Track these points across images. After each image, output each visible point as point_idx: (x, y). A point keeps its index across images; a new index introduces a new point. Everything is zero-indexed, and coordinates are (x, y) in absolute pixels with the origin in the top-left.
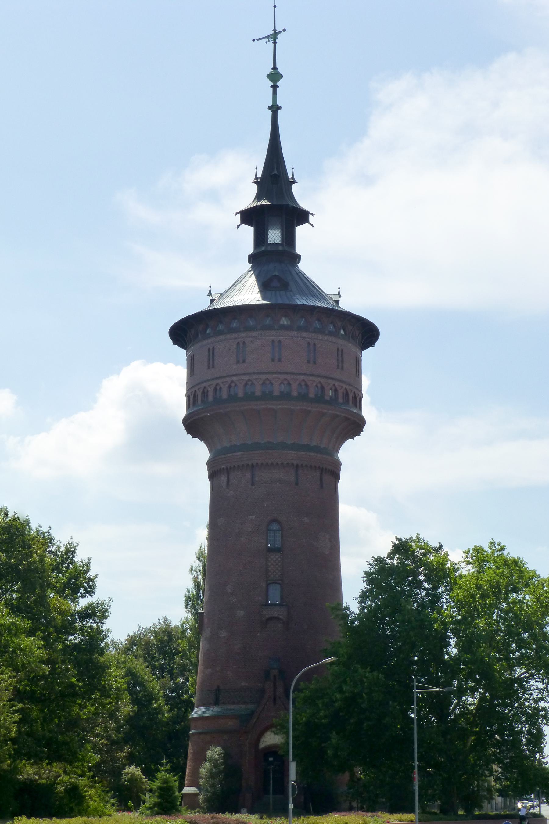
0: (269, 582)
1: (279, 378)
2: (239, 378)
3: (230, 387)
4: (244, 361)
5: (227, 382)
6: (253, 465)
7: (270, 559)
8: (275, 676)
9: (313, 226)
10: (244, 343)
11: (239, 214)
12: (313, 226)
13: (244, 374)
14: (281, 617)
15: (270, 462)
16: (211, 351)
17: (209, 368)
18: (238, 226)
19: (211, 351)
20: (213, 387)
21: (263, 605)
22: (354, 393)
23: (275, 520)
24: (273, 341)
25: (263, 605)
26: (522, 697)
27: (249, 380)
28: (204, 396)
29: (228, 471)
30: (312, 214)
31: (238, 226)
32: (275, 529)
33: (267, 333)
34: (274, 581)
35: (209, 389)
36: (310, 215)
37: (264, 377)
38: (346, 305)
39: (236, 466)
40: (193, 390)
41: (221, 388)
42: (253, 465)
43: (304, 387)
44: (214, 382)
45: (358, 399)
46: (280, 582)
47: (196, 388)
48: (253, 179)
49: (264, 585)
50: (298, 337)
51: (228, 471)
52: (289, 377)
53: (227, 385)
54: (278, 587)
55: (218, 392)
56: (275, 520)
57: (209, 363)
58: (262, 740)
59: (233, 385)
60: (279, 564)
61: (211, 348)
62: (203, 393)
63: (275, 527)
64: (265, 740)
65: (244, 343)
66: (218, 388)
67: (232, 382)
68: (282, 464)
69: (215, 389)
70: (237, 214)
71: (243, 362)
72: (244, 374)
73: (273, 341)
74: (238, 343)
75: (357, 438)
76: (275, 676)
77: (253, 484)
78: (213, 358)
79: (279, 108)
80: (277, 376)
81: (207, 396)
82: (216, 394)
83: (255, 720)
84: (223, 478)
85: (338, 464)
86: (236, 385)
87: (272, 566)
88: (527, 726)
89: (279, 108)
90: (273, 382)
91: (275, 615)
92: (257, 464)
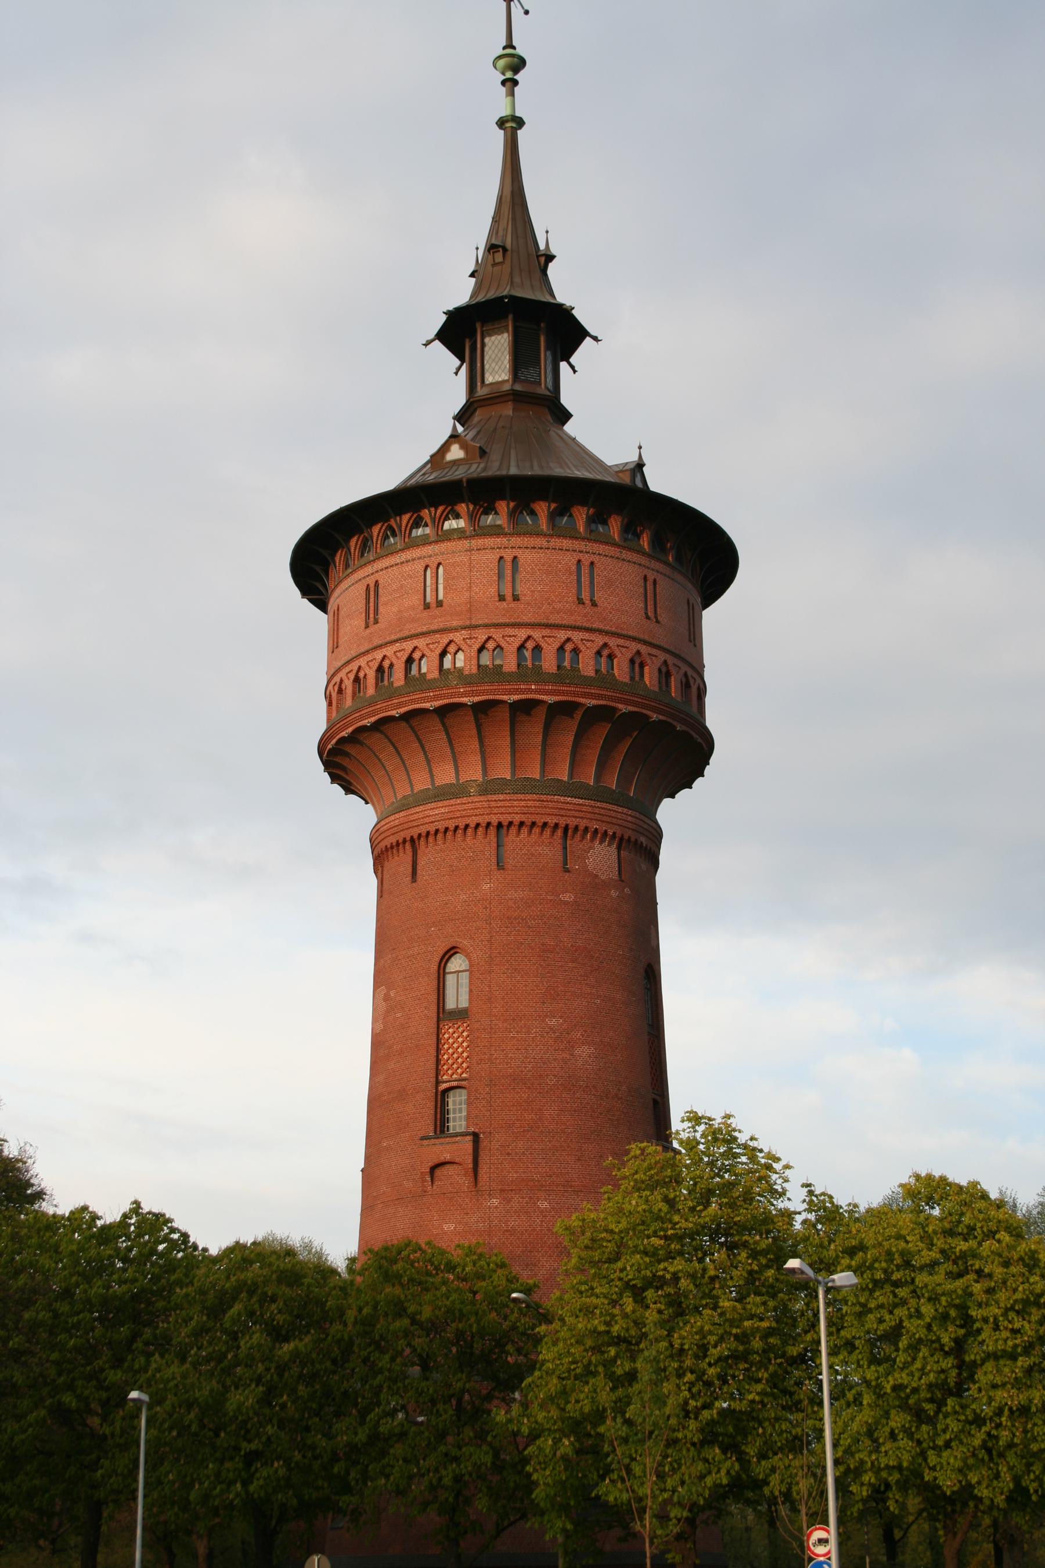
6: (500, 825)
17: (367, 627)
20: (375, 665)
22: (686, 675)
33: (489, 541)
38: (658, 482)
40: (337, 679)
41: (391, 665)
44: (409, 646)
45: (694, 689)
47: (362, 662)
53: (477, 646)
62: (357, 680)
75: (699, 782)
79: (520, 123)
84: (401, 862)
85: (657, 835)
89: (520, 123)
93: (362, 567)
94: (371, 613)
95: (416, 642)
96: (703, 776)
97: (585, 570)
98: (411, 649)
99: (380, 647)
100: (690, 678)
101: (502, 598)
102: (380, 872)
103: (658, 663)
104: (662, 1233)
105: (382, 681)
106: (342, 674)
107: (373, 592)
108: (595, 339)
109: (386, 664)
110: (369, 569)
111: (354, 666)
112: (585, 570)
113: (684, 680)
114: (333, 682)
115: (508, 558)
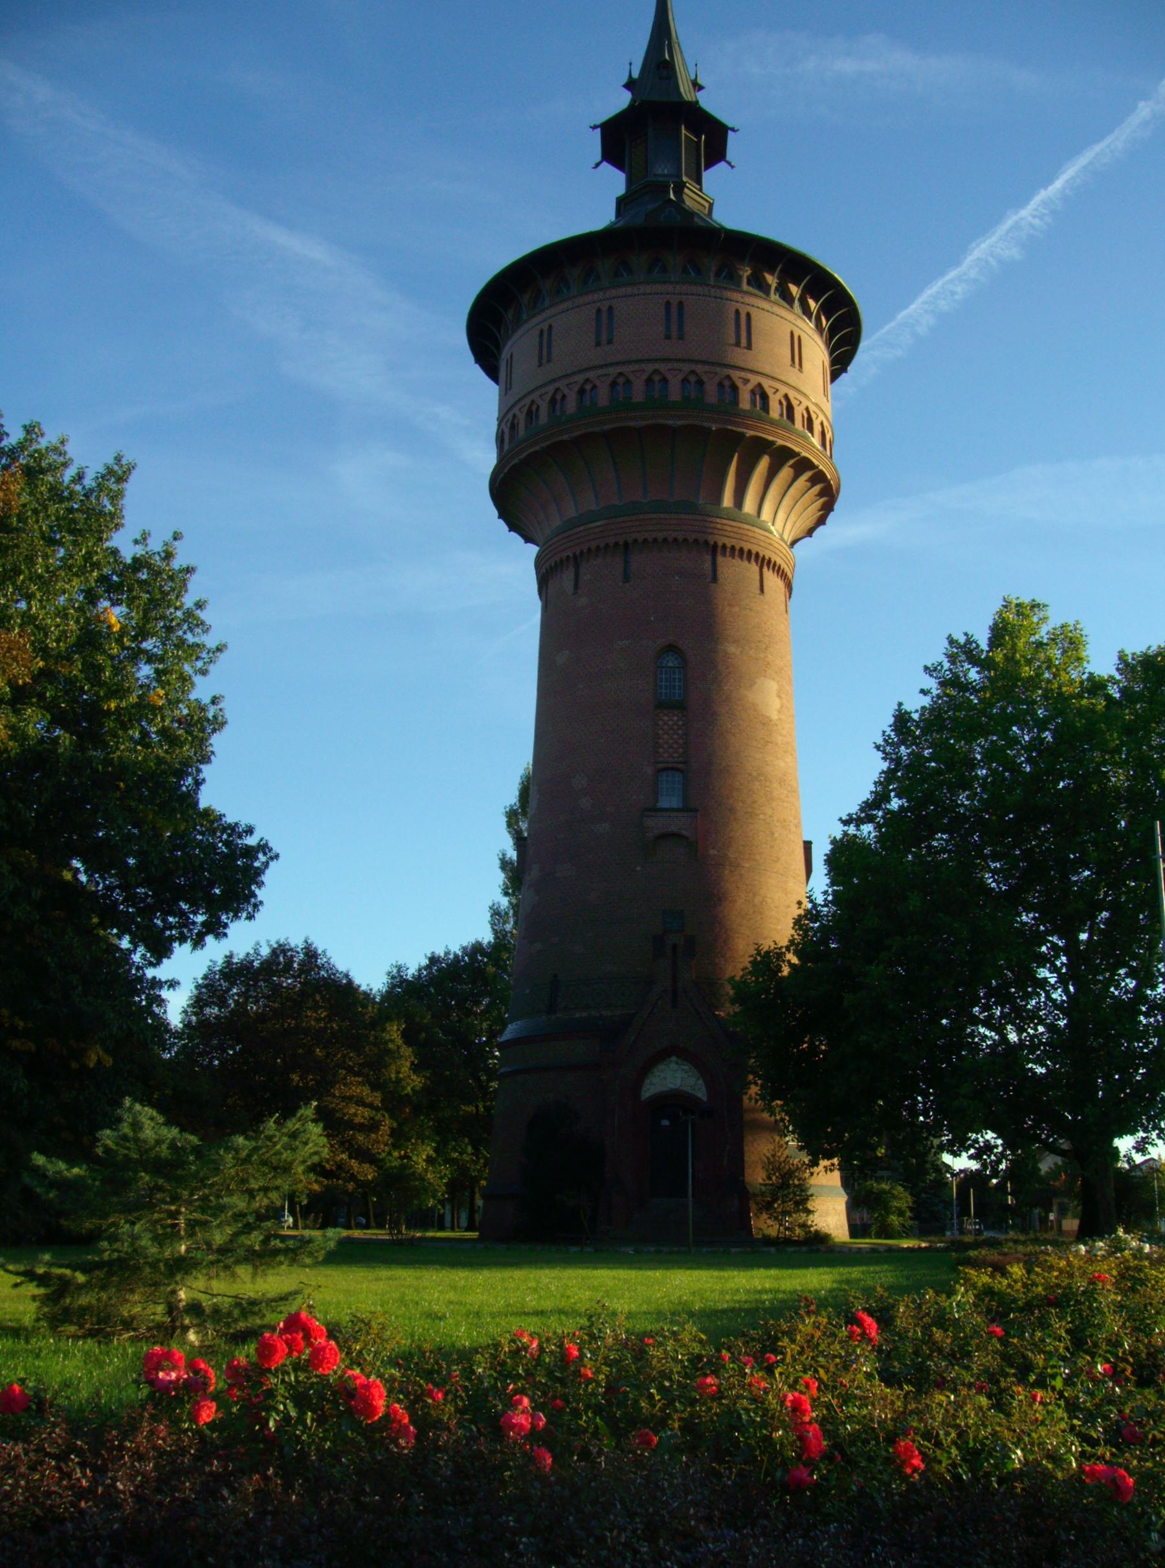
0: (661, 766)
1: (680, 370)
2: (600, 372)
3: (582, 391)
4: (610, 342)
5: (576, 382)
6: (626, 545)
7: (661, 723)
8: (675, 947)
9: (732, 167)
10: (610, 308)
11: (598, 131)
12: (732, 167)
13: (611, 365)
14: (684, 833)
15: (660, 536)
16: (545, 335)
18: (597, 165)
19: (545, 335)
20: (548, 397)
21: (649, 810)
22: (822, 424)
23: (671, 648)
24: (668, 304)
25: (649, 810)
26: (774, 1174)
27: (621, 374)
28: (532, 419)
29: (577, 561)
30: (733, 130)
31: (597, 165)
32: (670, 664)
34: (670, 765)
35: (540, 402)
36: (730, 132)
37: (650, 368)
39: (593, 548)
41: (564, 396)
42: (626, 545)
43: (728, 390)
44: (551, 389)
46: (680, 766)
48: (625, 80)
49: (649, 770)
50: (715, 297)
51: (576, 560)
52: (699, 369)
53: (576, 389)
54: (678, 777)
55: (558, 406)
56: (671, 648)
57: (540, 357)
58: (647, 1081)
59: (588, 387)
60: (680, 732)
61: (546, 328)
62: (529, 413)
63: (671, 661)
64: (741, 953)
65: (610, 308)
66: (559, 397)
67: (587, 380)
68: (685, 540)
69: (553, 401)
70: (594, 127)
71: (608, 343)
72: (611, 365)
73: (668, 304)
74: (599, 311)
76: (675, 947)
77: (626, 578)
78: (549, 346)
80: (676, 365)
81: (537, 417)
82: (554, 411)
83: (633, 1038)
84: (567, 579)
86: (594, 387)
87: (666, 736)
88: (23, 1423)
90: (669, 377)
91: (673, 828)
92: (636, 540)
93: (534, 316)
94: (545, 354)
95: (557, 385)
96: (499, 518)
97: (604, 316)
98: (553, 391)
99: (656, 361)
100: (811, 412)
101: (668, 337)
102: (544, 592)
103: (779, 396)
104: (752, 1414)
105: (531, 423)
106: (516, 410)
107: (546, 339)
108: (729, 163)
109: (534, 408)
110: (544, 315)
111: (528, 401)
112: (604, 316)
113: (806, 415)
114: (505, 420)
115: (674, 303)
